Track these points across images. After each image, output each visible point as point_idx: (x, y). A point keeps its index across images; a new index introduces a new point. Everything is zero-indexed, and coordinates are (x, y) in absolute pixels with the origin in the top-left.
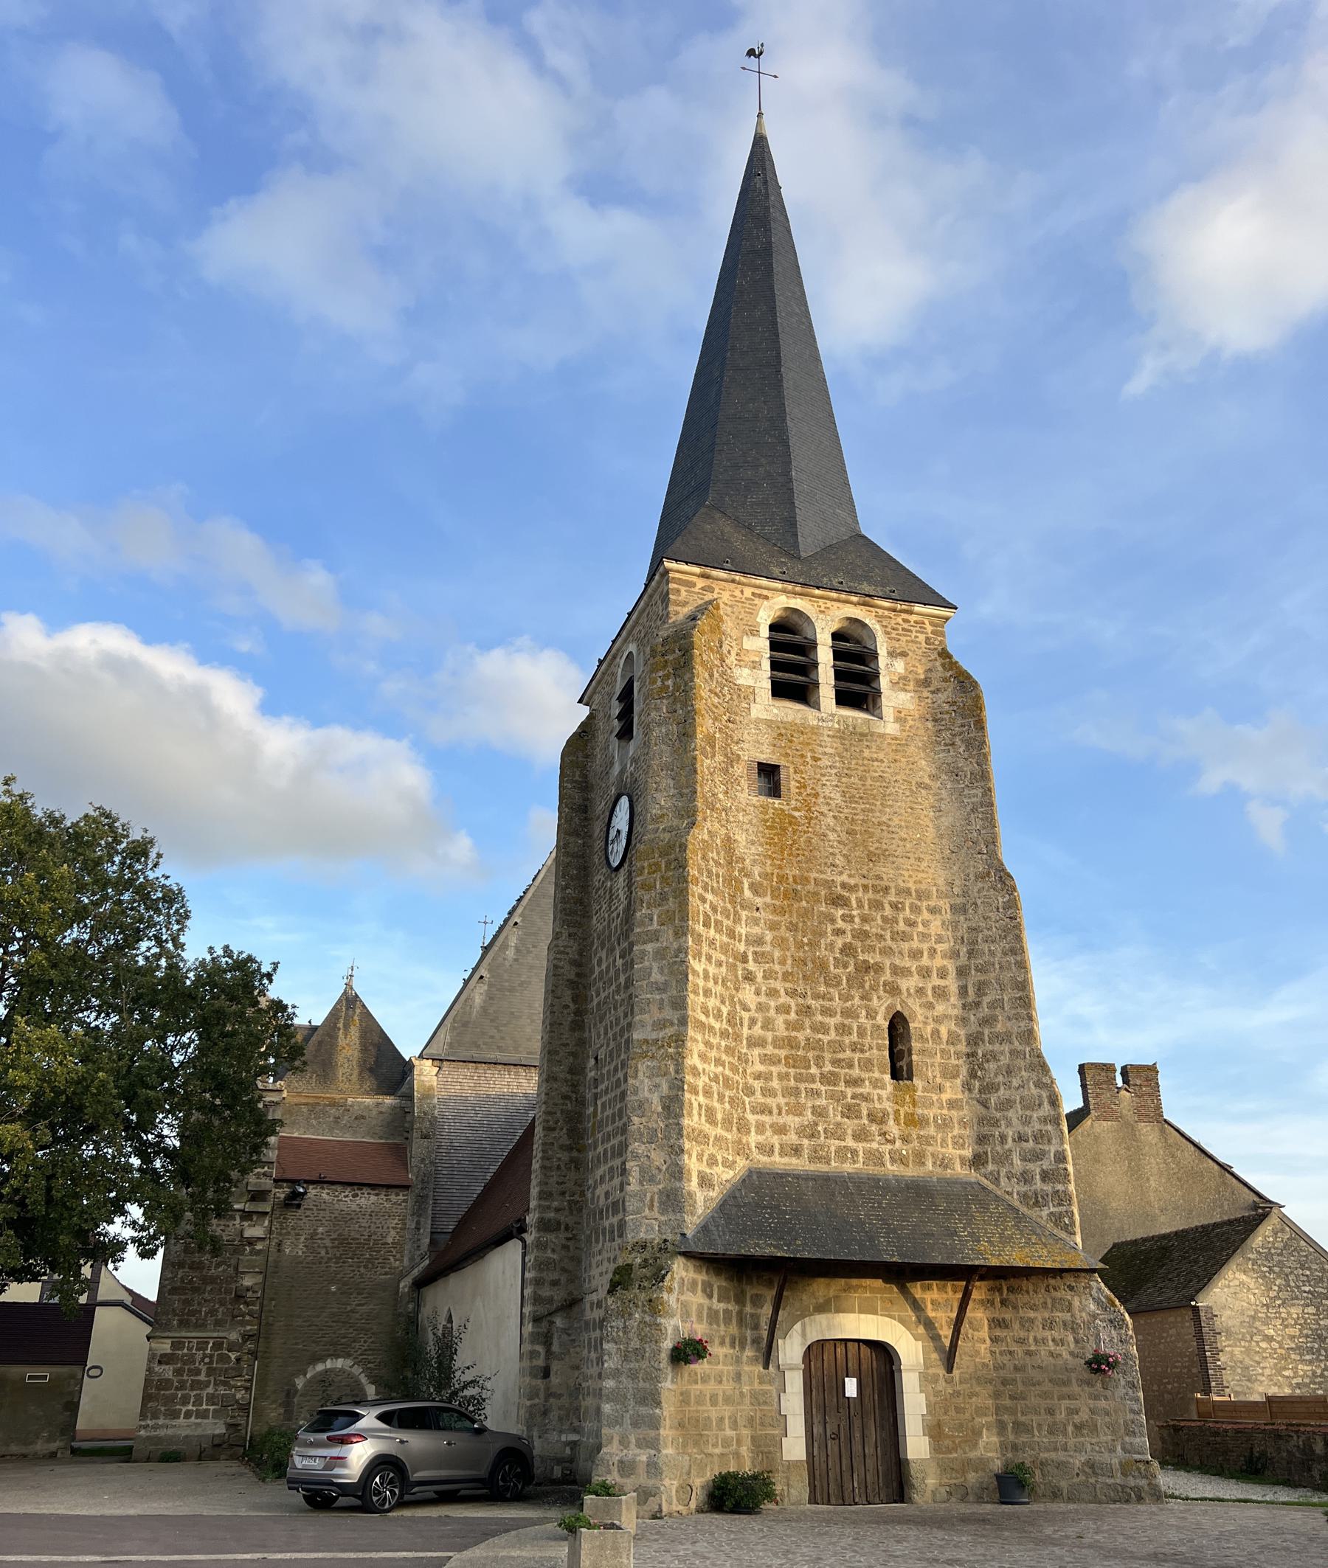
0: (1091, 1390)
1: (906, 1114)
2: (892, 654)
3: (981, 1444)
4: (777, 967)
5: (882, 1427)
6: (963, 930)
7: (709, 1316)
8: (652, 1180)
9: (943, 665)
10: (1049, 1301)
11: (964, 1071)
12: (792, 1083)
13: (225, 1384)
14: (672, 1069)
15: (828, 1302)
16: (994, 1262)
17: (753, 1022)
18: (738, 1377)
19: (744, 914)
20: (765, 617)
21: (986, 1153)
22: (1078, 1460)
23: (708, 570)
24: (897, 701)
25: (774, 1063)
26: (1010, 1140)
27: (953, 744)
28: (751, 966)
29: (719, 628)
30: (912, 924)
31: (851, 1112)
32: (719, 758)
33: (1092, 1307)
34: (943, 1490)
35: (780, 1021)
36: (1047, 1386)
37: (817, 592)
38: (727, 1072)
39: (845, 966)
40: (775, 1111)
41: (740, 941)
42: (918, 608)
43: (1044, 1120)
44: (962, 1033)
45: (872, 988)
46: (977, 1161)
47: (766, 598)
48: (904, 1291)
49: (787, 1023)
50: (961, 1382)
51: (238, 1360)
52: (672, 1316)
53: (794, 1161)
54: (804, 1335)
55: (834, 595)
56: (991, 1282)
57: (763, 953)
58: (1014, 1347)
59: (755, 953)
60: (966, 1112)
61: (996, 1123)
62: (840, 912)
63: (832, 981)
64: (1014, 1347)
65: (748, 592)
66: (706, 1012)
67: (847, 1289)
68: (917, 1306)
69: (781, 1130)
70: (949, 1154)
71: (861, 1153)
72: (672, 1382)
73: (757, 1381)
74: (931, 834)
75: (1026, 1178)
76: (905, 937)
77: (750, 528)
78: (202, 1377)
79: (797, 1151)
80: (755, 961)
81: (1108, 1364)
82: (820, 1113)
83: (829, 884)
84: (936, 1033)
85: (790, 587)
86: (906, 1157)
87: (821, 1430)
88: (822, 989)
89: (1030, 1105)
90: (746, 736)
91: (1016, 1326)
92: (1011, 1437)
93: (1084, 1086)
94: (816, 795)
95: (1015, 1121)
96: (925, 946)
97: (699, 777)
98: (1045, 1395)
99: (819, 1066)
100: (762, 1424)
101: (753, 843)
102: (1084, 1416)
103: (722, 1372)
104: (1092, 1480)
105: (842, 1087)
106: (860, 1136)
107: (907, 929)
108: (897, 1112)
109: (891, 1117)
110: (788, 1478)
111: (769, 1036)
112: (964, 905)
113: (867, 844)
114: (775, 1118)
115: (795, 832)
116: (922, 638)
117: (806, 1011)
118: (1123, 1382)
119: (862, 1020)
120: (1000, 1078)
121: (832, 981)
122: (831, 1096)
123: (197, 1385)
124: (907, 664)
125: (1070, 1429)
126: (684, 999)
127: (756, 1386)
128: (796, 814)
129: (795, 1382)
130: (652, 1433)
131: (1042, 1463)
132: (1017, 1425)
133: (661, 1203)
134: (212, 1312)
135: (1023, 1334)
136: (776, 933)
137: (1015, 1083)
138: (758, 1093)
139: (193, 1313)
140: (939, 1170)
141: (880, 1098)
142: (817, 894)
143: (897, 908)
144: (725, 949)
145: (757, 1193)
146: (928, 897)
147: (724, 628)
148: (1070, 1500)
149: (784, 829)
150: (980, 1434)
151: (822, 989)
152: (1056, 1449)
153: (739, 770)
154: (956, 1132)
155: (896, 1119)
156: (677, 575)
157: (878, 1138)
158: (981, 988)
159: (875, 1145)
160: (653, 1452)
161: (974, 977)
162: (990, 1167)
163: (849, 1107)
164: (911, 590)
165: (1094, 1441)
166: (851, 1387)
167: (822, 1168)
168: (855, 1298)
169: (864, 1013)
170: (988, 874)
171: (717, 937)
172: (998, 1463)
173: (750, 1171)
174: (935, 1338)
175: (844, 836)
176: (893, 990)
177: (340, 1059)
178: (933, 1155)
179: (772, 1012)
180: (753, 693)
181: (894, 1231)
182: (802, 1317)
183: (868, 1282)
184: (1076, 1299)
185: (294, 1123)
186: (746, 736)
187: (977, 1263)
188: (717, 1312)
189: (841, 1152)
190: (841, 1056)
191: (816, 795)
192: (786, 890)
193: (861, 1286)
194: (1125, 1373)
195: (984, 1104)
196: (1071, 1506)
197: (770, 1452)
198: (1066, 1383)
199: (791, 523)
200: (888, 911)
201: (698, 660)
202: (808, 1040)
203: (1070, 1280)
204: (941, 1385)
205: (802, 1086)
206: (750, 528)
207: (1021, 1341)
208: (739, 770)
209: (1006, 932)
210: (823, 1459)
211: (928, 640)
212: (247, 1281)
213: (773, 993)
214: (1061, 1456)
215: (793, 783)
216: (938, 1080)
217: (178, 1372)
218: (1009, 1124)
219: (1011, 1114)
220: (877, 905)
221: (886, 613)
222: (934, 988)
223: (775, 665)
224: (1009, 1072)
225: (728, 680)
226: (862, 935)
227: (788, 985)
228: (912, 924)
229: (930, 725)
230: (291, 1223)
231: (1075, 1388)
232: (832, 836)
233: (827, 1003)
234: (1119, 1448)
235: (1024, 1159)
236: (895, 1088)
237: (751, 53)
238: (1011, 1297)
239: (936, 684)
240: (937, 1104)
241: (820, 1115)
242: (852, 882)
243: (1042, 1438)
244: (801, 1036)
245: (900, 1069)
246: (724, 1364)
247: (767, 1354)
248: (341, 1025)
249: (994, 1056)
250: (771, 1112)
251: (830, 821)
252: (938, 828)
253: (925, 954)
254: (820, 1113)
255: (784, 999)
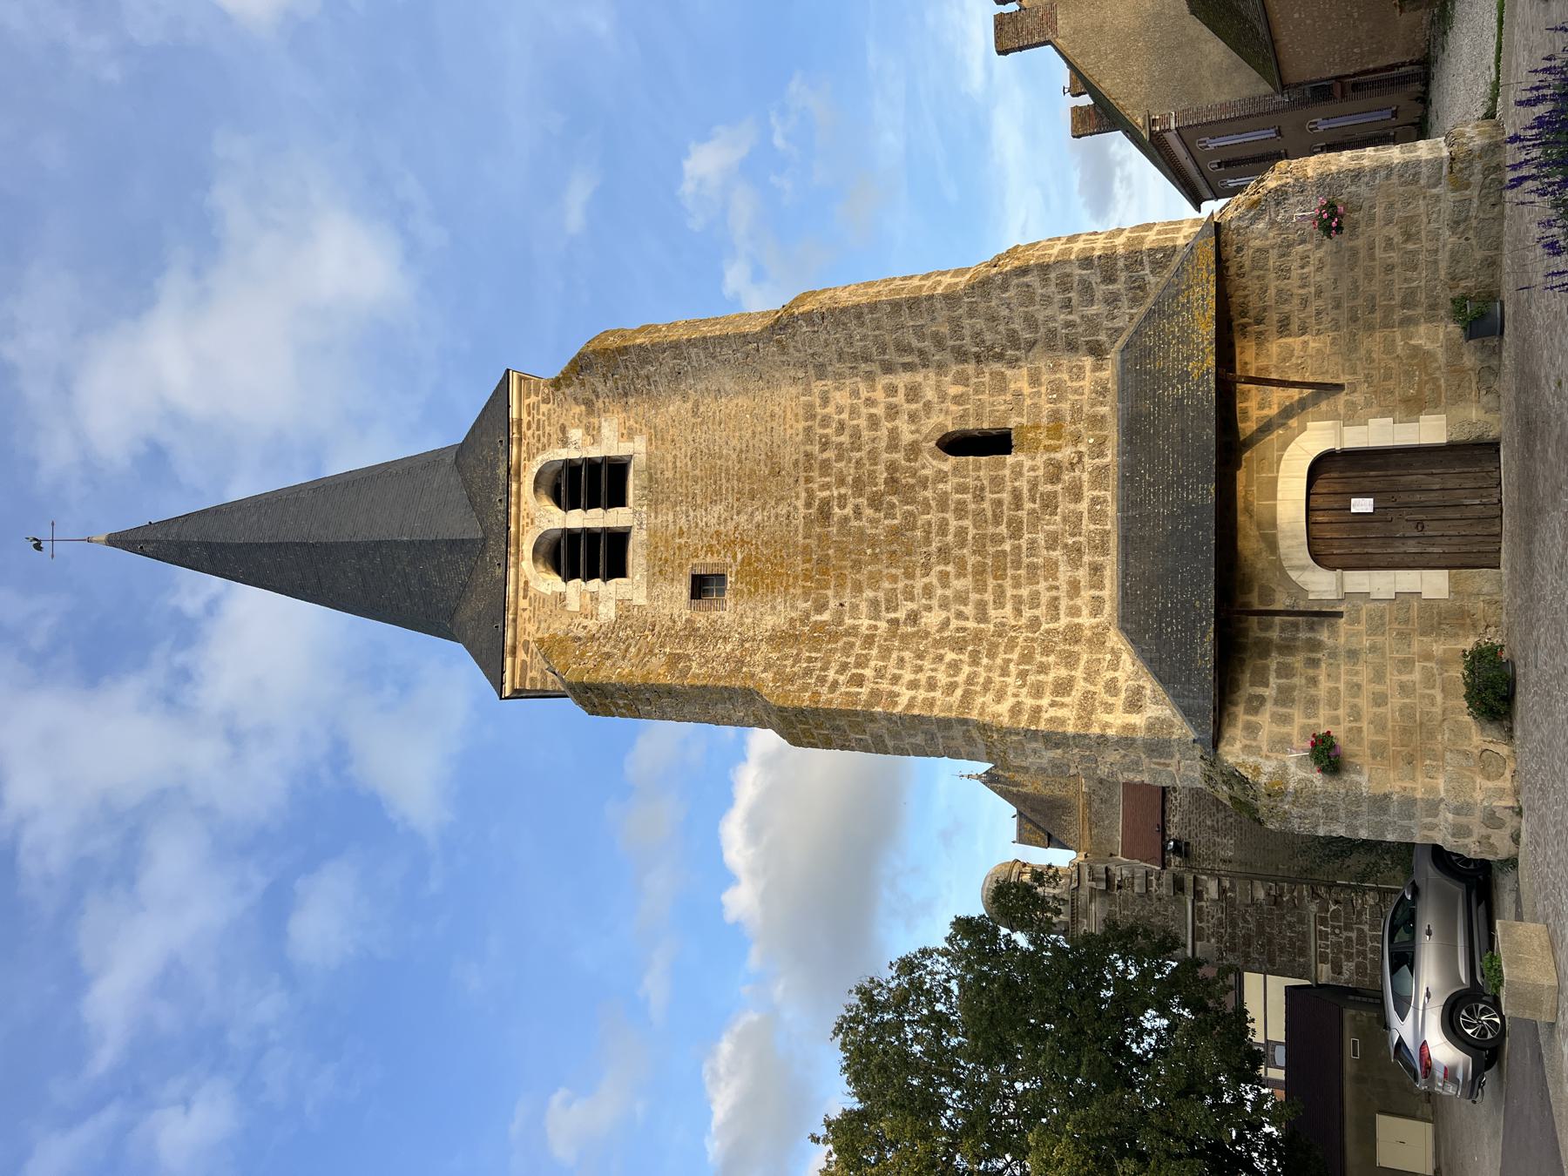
0: (1362, 224)
1: (1049, 437)
2: (565, 443)
3: (1428, 346)
4: (900, 585)
5: (1410, 466)
6: (843, 367)
7: (1284, 705)
8: (1137, 763)
9: (568, 386)
10: (1256, 273)
11: (997, 366)
12: (1022, 572)
13: (1360, 914)
14: (1015, 738)
15: (1264, 537)
16: (1211, 361)
17: (960, 615)
18: (1353, 654)
19: (848, 621)
20: (548, 583)
21: (1087, 343)
22: (1449, 239)
23: (508, 648)
24: (607, 439)
25: (1003, 592)
26: (1070, 317)
27: (648, 377)
28: (901, 615)
29: (561, 641)
30: (841, 427)
31: (1050, 504)
32: (690, 649)
33: (1261, 225)
34: (1484, 399)
35: (958, 584)
36: (1359, 272)
37: (513, 529)
38: (1015, 656)
39: (893, 506)
40: (1054, 593)
41: (876, 627)
42: (514, 414)
43: (1045, 281)
44: (955, 368)
45: (914, 475)
46: (1097, 351)
47: (526, 583)
48: (1249, 443)
49: (959, 576)
50: (1355, 373)
51: (1337, 902)
52: (1285, 768)
53: (1108, 573)
54: (1303, 568)
55: (513, 510)
56: (1237, 335)
57: (888, 601)
58: (1312, 309)
59: (887, 609)
60: (1042, 364)
61: (1052, 333)
62: (836, 510)
63: (910, 521)
64: (1312, 309)
65: (523, 603)
66: (952, 687)
67: (1248, 510)
68: (1266, 428)
69: (1074, 587)
70: (1090, 384)
71: (1096, 493)
72: (1360, 773)
73: (1356, 627)
74: (742, 401)
75: (1112, 300)
76: (856, 434)
77: (464, 585)
78: (1354, 935)
79: (1096, 569)
80: (895, 610)
81: (1331, 218)
82: (1053, 541)
83: (808, 521)
84: (958, 400)
85: (512, 559)
86: (1097, 438)
87: (1411, 542)
88: (919, 533)
89: (1028, 296)
90: (666, 611)
91: (1286, 308)
92: (1420, 310)
93: (1021, 49)
94: (718, 533)
95: (1049, 312)
96: (864, 411)
97: (711, 682)
98: (1369, 276)
99: (1002, 541)
100: (1407, 621)
101: (773, 608)
102: (1394, 232)
103: (1347, 683)
104: (1474, 223)
105: (1023, 514)
106: (1075, 493)
107: (847, 432)
108: (1048, 449)
109: (1052, 455)
110: (1470, 595)
111: (974, 596)
112: (815, 366)
113: (761, 478)
114: (1062, 593)
115: (758, 560)
116: (544, 408)
117: (944, 552)
118: (1353, 188)
119: (949, 487)
120: (1001, 328)
121: (910, 521)
122: (1034, 527)
123: (1361, 939)
124: (573, 426)
125: (1410, 246)
126: (939, 721)
127: (1362, 627)
128: (739, 557)
129: (1358, 581)
130: (1420, 804)
131: (1453, 279)
132: (1404, 305)
133: (1161, 756)
134: (1291, 926)
135: (1296, 301)
136: (865, 585)
137: (1006, 312)
138: (1037, 612)
139: (1292, 944)
140: (1109, 398)
141: (1033, 469)
142: (819, 537)
143: (826, 443)
144: (885, 653)
145: (1146, 631)
146: (811, 406)
147: (561, 634)
148: (1498, 247)
149: (756, 573)
150: (1416, 348)
151: (919, 533)
152: (1436, 262)
153: (701, 620)
154: (1066, 377)
155: (1055, 449)
156: (517, 680)
157: (1077, 473)
158: (903, 349)
159: (1085, 477)
160: (1442, 806)
161: (891, 355)
162: (1103, 337)
163: (1045, 506)
164: (495, 414)
165: (1425, 220)
166: (1362, 505)
167: (1113, 542)
168: (1259, 504)
169: (941, 486)
170: (779, 342)
171: (872, 664)
172: (1451, 326)
173: (1123, 629)
174: (1302, 405)
175: (757, 503)
176: (914, 450)
177: (1046, 792)
178: (1093, 406)
179: (949, 592)
180: (622, 601)
181: (1180, 477)
182: (1282, 569)
183: (1240, 488)
184: (1252, 243)
185: (1109, 841)
186: (666, 611)
187: (1213, 385)
188: (1280, 689)
189: (1097, 517)
190: (989, 514)
191: (718, 533)
192: (819, 572)
193: (1245, 497)
194: (1342, 187)
195: (1032, 344)
196: (1507, 248)
197: (1439, 614)
198: (1354, 252)
199: (453, 544)
200: (830, 454)
201: (594, 676)
202: (974, 552)
203: (1230, 251)
204: (1358, 397)
205: (1026, 561)
206: (464, 585)
207: (1305, 302)
208: (701, 620)
209: (837, 323)
210: (1446, 540)
211: (546, 401)
212: (1260, 894)
213: (928, 591)
214: (1444, 258)
215: (709, 560)
216: (1009, 397)
217: (1349, 957)
218: (1052, 318)
219: (1040, 317)
220: (825, 467)
221: (524, 448)
222: (908, 401)
223: (591, 575)
224: (993, 319)
225: (610, 632)
226: (858, 486)
227: (918, 572)
228: (841, 427)
229: (631, 401)
230: (1203, 851)
231: (1360, 242)
232: (758, 517)
233: (934, 529)
234: (1434, 191)
235: (1092, 302)
236: (1021, 450)
237: (38, 547)
238: (1252, 313)
239: (589, 394)
240: (1036, 400)
241: (1055, 540)
242: (803, 495)
243: (1420, 279)
244: (972, 560)
245: (996, 443)
246: (1338, 680)
247: (1324, 615)
248: (1015, 789)
249: (977, 335)
250: (1056, 598)
251: (743, 518)
252: (737, 393)
253: (873, 411)
254: (1053, 541)
255: (933, 579)
